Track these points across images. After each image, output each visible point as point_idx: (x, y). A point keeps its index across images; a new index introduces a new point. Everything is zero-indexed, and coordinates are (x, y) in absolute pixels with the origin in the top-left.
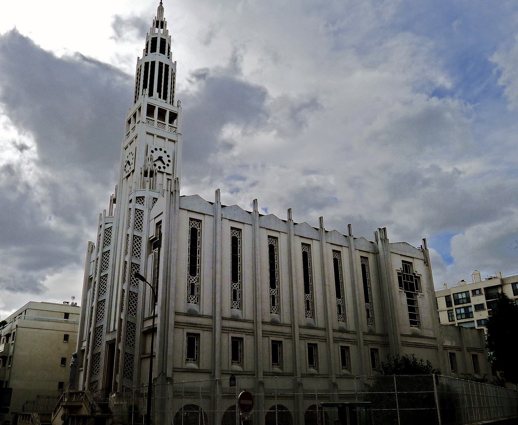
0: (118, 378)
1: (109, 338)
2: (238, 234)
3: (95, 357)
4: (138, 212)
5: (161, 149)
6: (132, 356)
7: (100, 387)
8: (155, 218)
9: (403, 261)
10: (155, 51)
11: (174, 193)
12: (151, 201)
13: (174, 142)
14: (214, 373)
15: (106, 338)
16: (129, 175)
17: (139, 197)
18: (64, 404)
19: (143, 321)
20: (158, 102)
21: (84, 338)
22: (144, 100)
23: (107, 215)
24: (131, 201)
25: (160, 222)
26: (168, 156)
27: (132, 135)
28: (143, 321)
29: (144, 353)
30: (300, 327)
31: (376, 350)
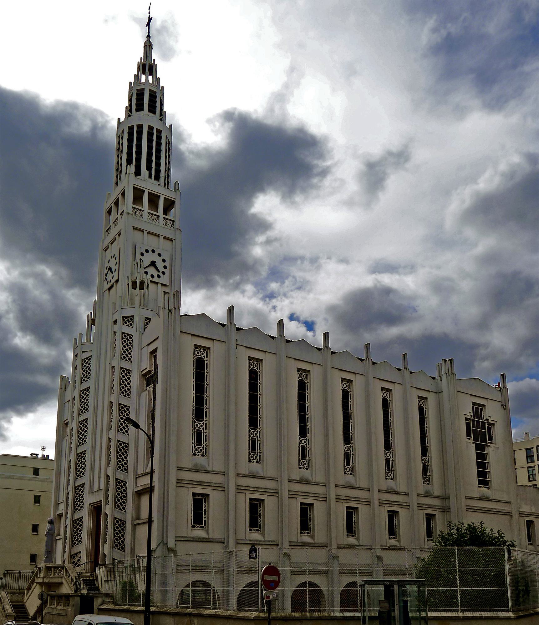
0: (106, 548)
1: (93, 499)
2: (258, 366)
3: (77, 523)
4: (125, 336)
5: (153, 251)
6: (124, 523)
7: (84, 560)
8: (148, 345)
9: (473, 404)
10: (142, 109)
11: (173, 311)
12: (143, 323)
13: (171, 240)
14: (228, 542)
15: (89, 499)
16: (112, 287)
17: (126, 317)
18: (40, 580)
19: (137, 478)
20: (149, 185)
21: (61, 500)
22: (129, 182)
23: (84, 341)
24: (115, 322)
25: (155, 350)
26: (164, 261)
27: (114, 232)
28: (137, 478)
29: (138, 518)
30: (337, 486)
31: (434, 515)
